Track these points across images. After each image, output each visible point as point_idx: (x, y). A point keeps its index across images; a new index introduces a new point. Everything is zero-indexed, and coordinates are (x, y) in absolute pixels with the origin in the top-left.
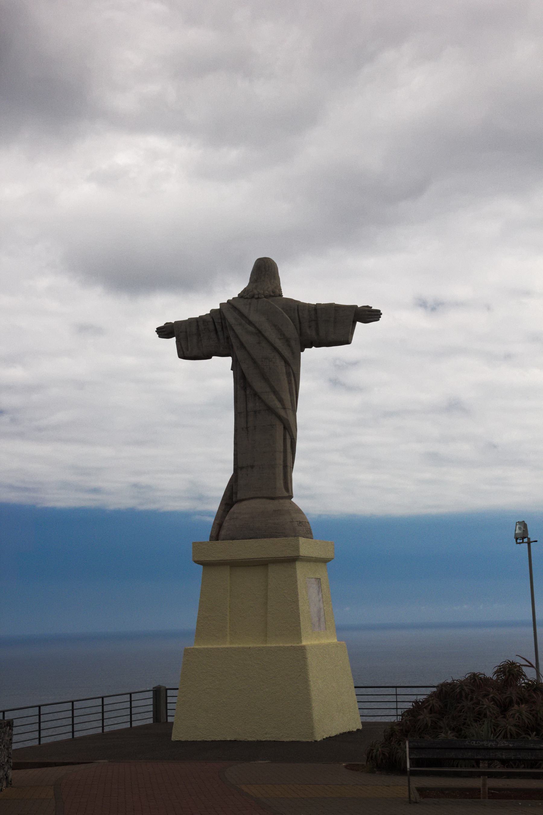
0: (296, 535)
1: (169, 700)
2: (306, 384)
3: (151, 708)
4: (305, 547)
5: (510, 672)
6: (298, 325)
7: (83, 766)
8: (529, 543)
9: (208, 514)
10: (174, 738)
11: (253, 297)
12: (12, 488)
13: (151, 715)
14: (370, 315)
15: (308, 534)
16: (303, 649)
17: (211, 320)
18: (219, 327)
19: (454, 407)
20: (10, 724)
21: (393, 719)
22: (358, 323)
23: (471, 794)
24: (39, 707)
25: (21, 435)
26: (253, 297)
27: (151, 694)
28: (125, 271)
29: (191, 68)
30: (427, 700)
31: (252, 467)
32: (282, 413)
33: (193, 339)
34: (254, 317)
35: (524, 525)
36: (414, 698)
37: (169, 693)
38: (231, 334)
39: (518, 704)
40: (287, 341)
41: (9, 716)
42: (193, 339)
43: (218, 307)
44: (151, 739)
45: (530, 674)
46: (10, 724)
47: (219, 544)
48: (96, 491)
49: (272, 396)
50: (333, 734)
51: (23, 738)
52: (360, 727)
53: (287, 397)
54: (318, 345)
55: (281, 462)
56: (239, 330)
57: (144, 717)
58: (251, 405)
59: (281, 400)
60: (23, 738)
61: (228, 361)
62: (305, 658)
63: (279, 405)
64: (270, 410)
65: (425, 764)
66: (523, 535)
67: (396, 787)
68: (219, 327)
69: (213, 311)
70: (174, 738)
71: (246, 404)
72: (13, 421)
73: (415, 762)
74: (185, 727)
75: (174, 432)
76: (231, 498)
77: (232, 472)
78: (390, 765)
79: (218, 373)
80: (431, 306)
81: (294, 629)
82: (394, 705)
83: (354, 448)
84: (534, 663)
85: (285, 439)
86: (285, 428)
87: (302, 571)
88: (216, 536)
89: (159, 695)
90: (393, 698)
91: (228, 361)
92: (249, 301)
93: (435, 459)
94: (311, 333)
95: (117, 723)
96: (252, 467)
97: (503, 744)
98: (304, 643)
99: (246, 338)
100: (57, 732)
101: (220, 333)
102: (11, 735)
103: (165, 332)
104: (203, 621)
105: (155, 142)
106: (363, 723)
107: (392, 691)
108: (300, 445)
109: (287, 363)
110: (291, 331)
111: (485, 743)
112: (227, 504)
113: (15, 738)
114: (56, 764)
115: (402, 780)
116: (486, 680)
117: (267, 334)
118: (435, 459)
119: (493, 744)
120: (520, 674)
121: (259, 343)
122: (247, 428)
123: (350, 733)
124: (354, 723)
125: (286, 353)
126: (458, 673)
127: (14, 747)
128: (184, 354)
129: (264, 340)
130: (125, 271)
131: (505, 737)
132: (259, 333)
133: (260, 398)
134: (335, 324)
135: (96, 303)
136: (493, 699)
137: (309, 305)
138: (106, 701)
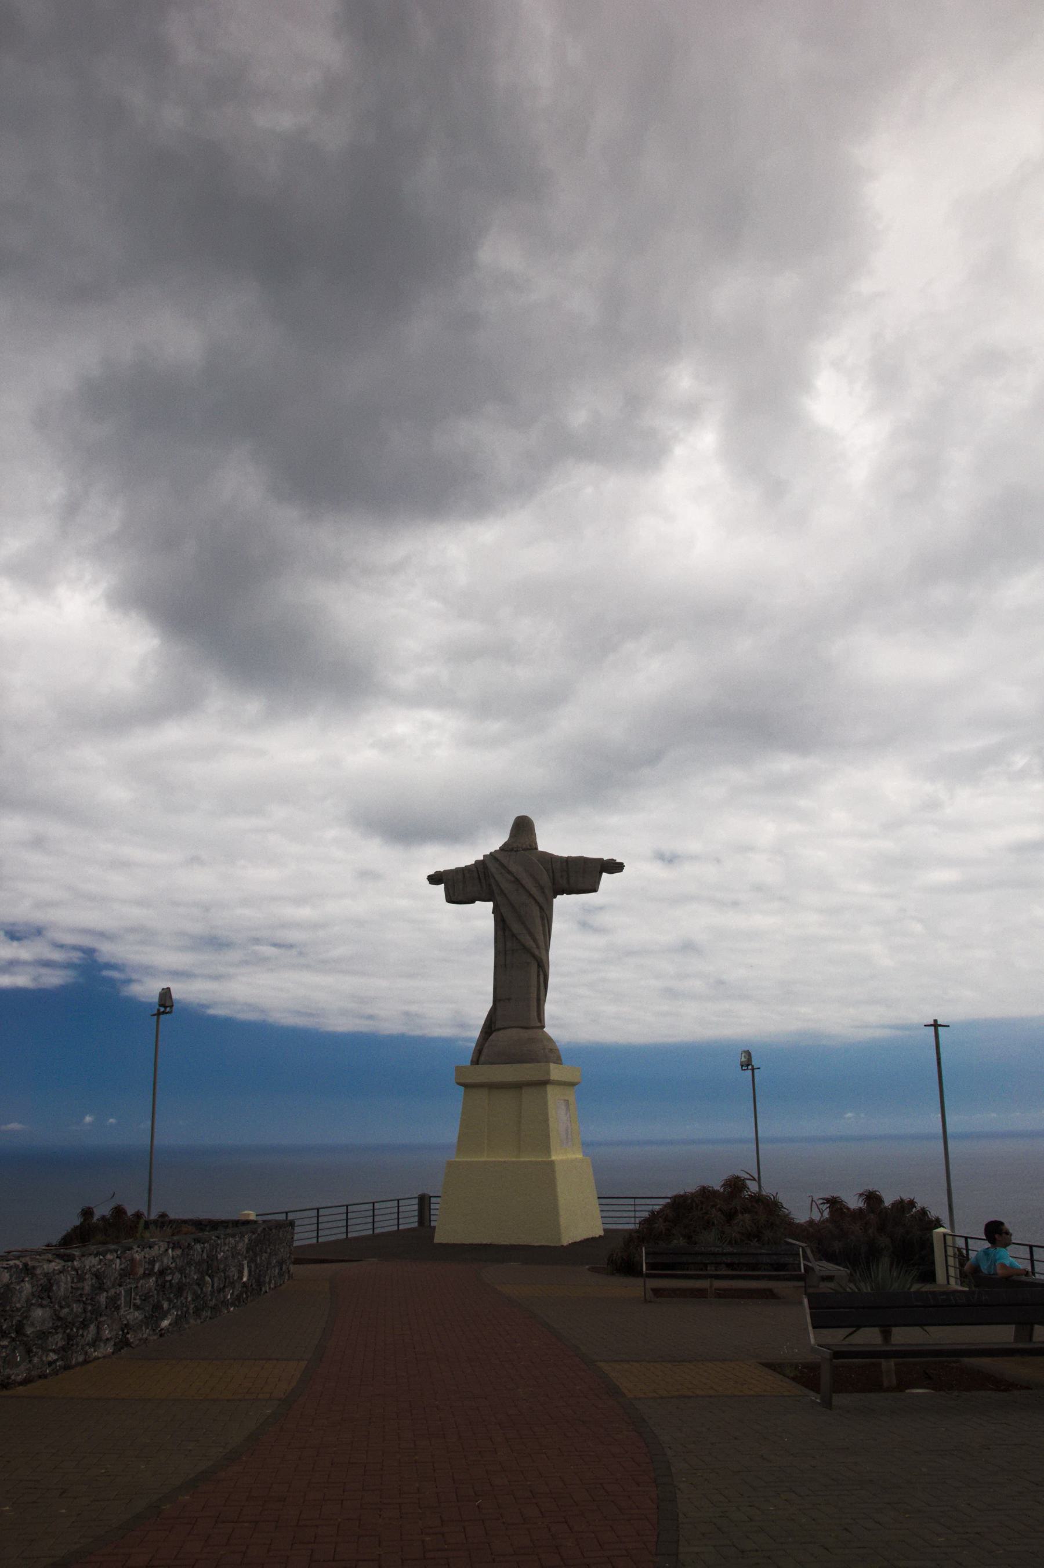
0: (548, 1061)
1: (432, 1206)
2: (557, 926)
3: (416, 1213)
4: (555, 1072)
5: (735, 1185)
7: (355, 1264)
8: (753, 1070)
9: (468, 1039)
10: (437, 1240)
11: (512, 850)
12: (298, 1013)
13: (416, 1219)
14: (615, 867)
15: (558, 1060)
16: (552, 1163)
19: (688, 947)
20: (292, 1224)
21: (631, 1227)
22: (604, 874)
23: (699, 1294)
24: (318, 1210)
25: (307, 967)
27: (416, 1201)
28: (402, 825)
29: (461, 654)
30: (661, 1211)
31: (509, 999)
32: (537, 952)
33: (460, 886)
34: (513, 868)
35: (748, 1054)
36: (650, 1208)
37: (433, 1200)
39: (742, 1213)
40: (542, 889)
41: (291, 1217)
42: (460, 886)
43: (482, 858)
44: (415, 1241)
45: (753, 1187)
46: (292, 1224)
47: (482, 1068)
48: (370, 1017)
49: (528, 937)
50: (578, 1239)
51: (303, 1236)
52: (602, 1233)
53: (540, 938)
54: (569, 893)
55: (535, 995)
56: (498, 877)
57: (410, 1222)
59: (535, 941)
60: (303, 1236)
61: (490, 905)
62: (553, 1171)
64: (527, 950)
65: (661, 1267)
66: (747, 1063)
67: (633, 1288)
69: (477, 862)
70: (437, 1240)
72: (301, 954)
73: (651, 1266)
74: (448, 1230)
75: (441, 971)
76: (490, 1027)
77: (489, 1005)
78: (627, 1267)
79: (481, 915)
80: (668, 859)
81: (545, 1147)
82: (632, 1214)
83: (601, 982)
84: (756, 1177)
85: (538, 976)
87: (552, 1094)
88: (476, 1061)
89: (424, 1202)
90: (632, 1208)
91: (490, 905)
93: (670, 993)
95: (386, 1225)
96: (509, 999)
97: (729, 1249)
98: (553, 1158)
100: (332, 1233)
101: (483, 881)
102: (293, 1234)
103: (435, 879)
104: (462, 1136)
105: (430, 715)
106: (605, 1230)
107: (631, 1201)
108: (552, 980)
109: (541, 908)
110: (545, 879)
111: (713, 1249)
112: (486, 1033)
113: (295, 1238)
114: (332, 1261)
115: (640, 1281)
116: (715, 1193)
117: (524, 882)
118: (670, 993)
119: (720, 1250)
120: (744, 1187)
123: (593, 1239)
124: (596, 1230)
125: (540, 899)
126: (689, 1186)
127: (296, 1244)
128: (451, 899)
129: (520, 888)
130: (402, 825)
131: (730, 1243)
132: (517, 881)
134: (583, 875)
135: (375, 852)
136: (720, 1210)
137: (561, 857)
138: (321, 1212)
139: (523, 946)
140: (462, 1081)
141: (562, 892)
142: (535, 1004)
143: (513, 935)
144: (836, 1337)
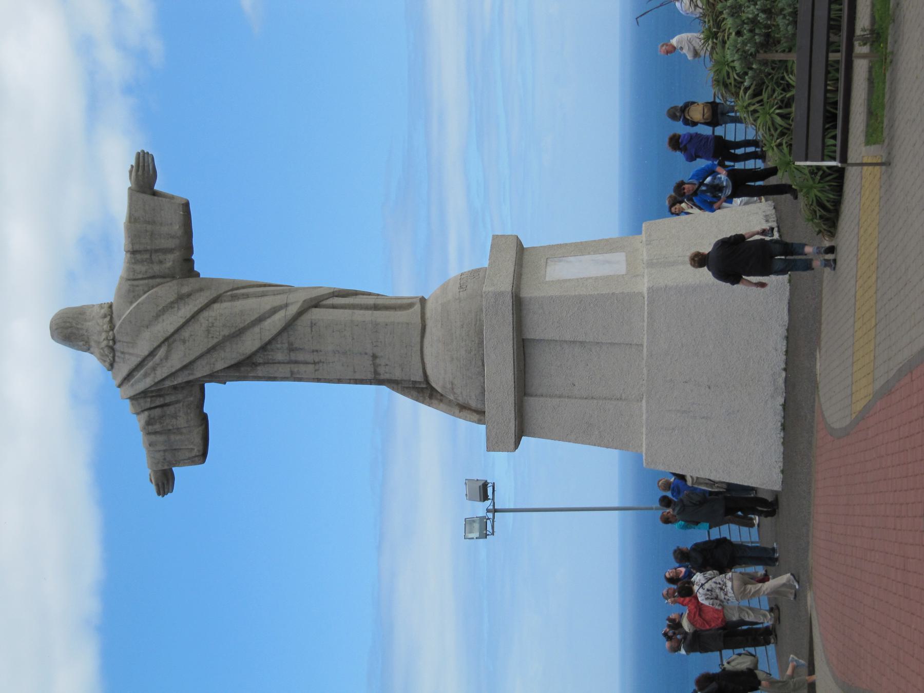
6: (158, 280)
11: (112, 349)
16: (651, 290)
17: (146, 413)
18: (159, 401)
26: (112, 349)
31: (374, 357)
32: (293, 310)
34: (143, 348)
38: (168, 383)
40: (182, 298)
49: (267, 323)
53: (253, 306)
55: (368, 315)
56: (161, 373)
58: (280, 356)
63: (280, 315)
64: (290, 325)
67: (860, 188)
68: (159, 401)
71: (279, 363)
85: (334, 307)
86: (316, 306)
88: (479, 414)
92: (118, 354)
94: (170, 261)
96: (374, 357)
99: (176, 361)
101: (168, 399)
103: (164, 482)
109: (215, 301)
110: (167, 291)
112: (431, 397)
115: (852, 176)
121: (184, 341)
122: (315, 363)
132: (168, 340)
133: (269, 342)
139: (280, 333)
140: (513, 446)
141: (187, 262)
142: (377, 313)
143: (264, 348)
144: (643, 232)
